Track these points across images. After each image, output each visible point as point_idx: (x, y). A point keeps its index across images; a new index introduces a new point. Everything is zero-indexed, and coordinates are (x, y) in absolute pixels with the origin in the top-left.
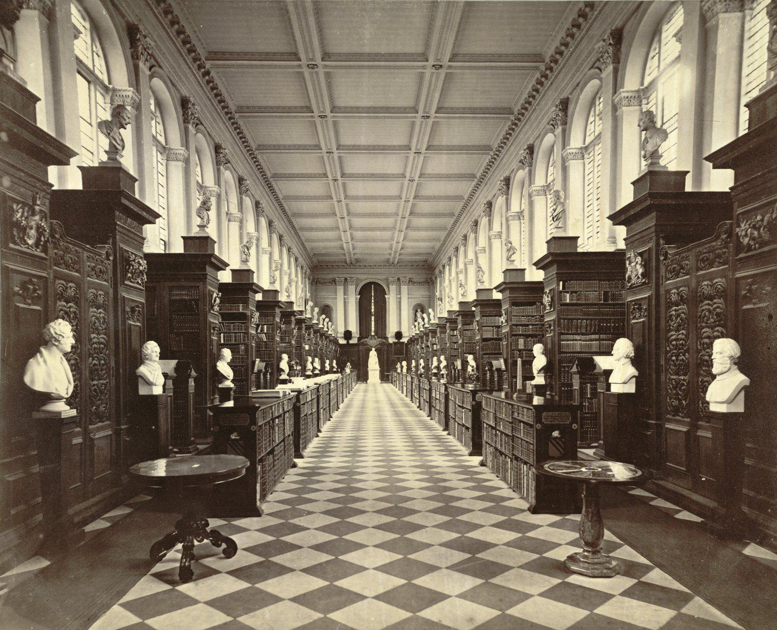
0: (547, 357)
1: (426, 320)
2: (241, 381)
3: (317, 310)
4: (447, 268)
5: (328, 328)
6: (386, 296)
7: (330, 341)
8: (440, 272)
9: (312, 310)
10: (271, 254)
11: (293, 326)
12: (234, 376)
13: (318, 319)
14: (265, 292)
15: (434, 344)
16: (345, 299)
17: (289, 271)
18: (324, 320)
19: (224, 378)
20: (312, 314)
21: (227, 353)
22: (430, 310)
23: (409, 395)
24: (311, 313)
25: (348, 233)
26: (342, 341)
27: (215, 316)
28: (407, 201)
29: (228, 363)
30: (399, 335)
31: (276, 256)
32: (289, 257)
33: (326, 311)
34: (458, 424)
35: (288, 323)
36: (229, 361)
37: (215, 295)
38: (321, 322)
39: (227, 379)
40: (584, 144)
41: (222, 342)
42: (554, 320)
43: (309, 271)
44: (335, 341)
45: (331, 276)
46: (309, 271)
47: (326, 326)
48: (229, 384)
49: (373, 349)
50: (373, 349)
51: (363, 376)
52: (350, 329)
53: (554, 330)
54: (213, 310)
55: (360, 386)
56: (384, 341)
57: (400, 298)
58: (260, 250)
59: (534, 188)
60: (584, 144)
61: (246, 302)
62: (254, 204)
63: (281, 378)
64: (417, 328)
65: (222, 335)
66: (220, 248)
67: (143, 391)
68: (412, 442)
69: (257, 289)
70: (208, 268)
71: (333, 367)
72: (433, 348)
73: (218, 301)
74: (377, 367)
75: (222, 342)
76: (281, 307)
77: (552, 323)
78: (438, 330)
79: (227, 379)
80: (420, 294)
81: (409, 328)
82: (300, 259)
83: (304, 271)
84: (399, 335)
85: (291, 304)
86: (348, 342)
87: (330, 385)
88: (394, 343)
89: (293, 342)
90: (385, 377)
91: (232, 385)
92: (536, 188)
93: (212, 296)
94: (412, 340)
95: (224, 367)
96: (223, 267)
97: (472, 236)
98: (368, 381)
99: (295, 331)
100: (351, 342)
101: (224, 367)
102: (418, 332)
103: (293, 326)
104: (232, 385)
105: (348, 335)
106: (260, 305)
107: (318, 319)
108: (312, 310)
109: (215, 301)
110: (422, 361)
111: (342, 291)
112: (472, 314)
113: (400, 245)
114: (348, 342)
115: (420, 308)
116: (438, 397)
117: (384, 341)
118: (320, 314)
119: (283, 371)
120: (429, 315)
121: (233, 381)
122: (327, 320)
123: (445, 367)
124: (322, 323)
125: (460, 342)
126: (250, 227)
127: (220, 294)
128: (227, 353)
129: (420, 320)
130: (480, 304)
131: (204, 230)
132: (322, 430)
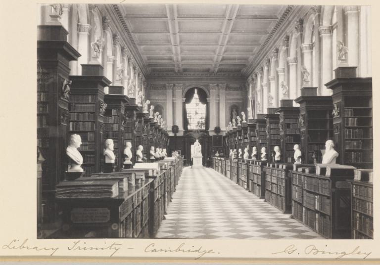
0: (301, 150)
1: (244, 117)
2: (90, 165)
3: (152, 107)
4: (259, 76)
5: (160, 123)
6: (208, 99)
7: (162, 133)
8: (253, 80)
9: (149, 108)
10: (114, 61)
11: (135, 119)
12: (84, 162)
13: (153, 115)
14: (112, 89)
15: (251, 137)
16: (173, 100)
17: (128, 77)
18: (158, 116)
19: (73, 163)
20: (149, 110)
21: (77, 139)
22: (243, 113)
23: (235, 178)
24: (146, 108)
25: (179, 48)
26: (171, 134)
27: (64, 103)
28: (230, 20)
29: (78, 149)
30: (217, 130)
31: (119, 65)
32: (129, 65)
33: (159, 109)
34: (307, 209)
35: (131, 116)
36: (79, 146)
37: (65, 82)
38: (156, 118)
39: (77, 164)
40: (331, 24)
41: (71, 129)
42: (340, 123)
43: (144, 77)
44: (167, 135)
45: (162, 83)
46: (144, 79)
47: (159, 121)
48: (79, 169)
49: (197, 140)
50: (197, 140)
51: (188, 161)
52: (177, 125)
53: (305, 136)
54: (63, 96)
55: (186, 169)
56: (206, 134)
57: (219, 100)
58: (106, 58)
59: (322, 28)
60: (331, 24)
61: (95, 93)
62: (101, 18)
63: (125, 163)
64: (234, 124)
65: (71, 123)
66: (71, 37)
67: (107, 161)
68: (261, 226)
69: (104, 82)
70: (59, 56)
71: (138, 156)
72: (251, 139)
73: (68, 88)
74: (200, 155)
75: (71, 129)
76: (126, 102)
77: (339, 125)
78: (257, 124)
79: (77, 164)
80: (235, 97)
81: (227, 124)
82: (137, 68)
83: (140, 78)
84: (217, 130)
85: (134, 99)
86: (175, 135)
87: (171, 170)
88: (214, 136)
89: (135, 133)
90: (208, 162)
91: (82, 170)
92: (323, 28)
93: (62, 83)
94: (231, 134)
95: (74, 153)
96: (76, 57)
97: (284, 48)
98: (193, 166)
99: (137, 123)
100: (178, 135)
101: (74, 153)
102: (235, 127)
103: (135, 119)
104: (82, 170)
105: (175, 129)
106: (107, 98)
107: (153, 115)
108: (149, 108)
109: (65, 88)
110: (263, 150)
111: (171, 94)
112: (277, 117)
113: (220, 58)
114: (175, 135)
115: (237, 109)
116: (275, 181)
117: (206, 134)
118: (155, 111)
119: (126, 156)
120: (241, 117)
121: (83, 166)
122: (160, 116)
123: (255, 155)
124: (157, 119)
125: (282, 134)
126: (97, 36)
127: (71, 82)
128: (77, 139)
129: (234, 120)
130: (306, 101)
131: (57, 20)
132: (167, 212)
